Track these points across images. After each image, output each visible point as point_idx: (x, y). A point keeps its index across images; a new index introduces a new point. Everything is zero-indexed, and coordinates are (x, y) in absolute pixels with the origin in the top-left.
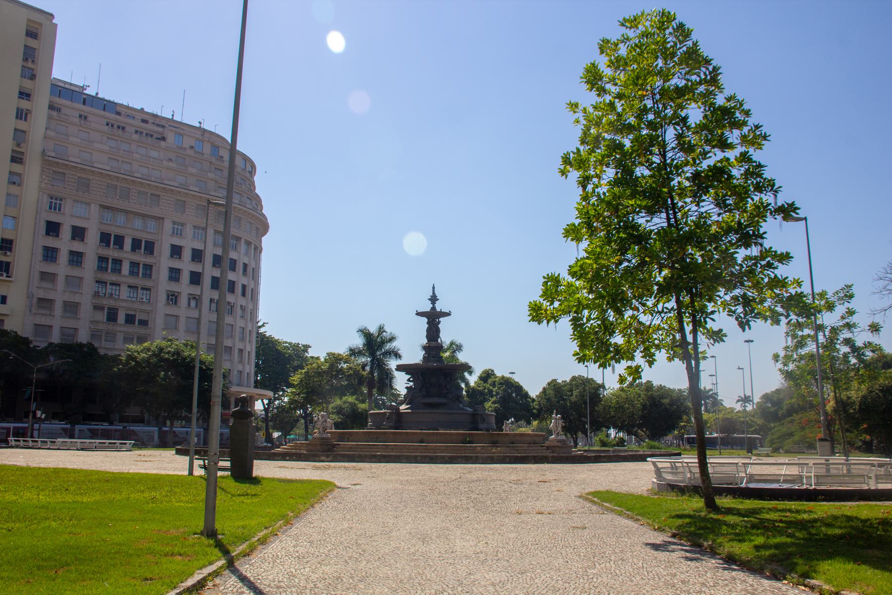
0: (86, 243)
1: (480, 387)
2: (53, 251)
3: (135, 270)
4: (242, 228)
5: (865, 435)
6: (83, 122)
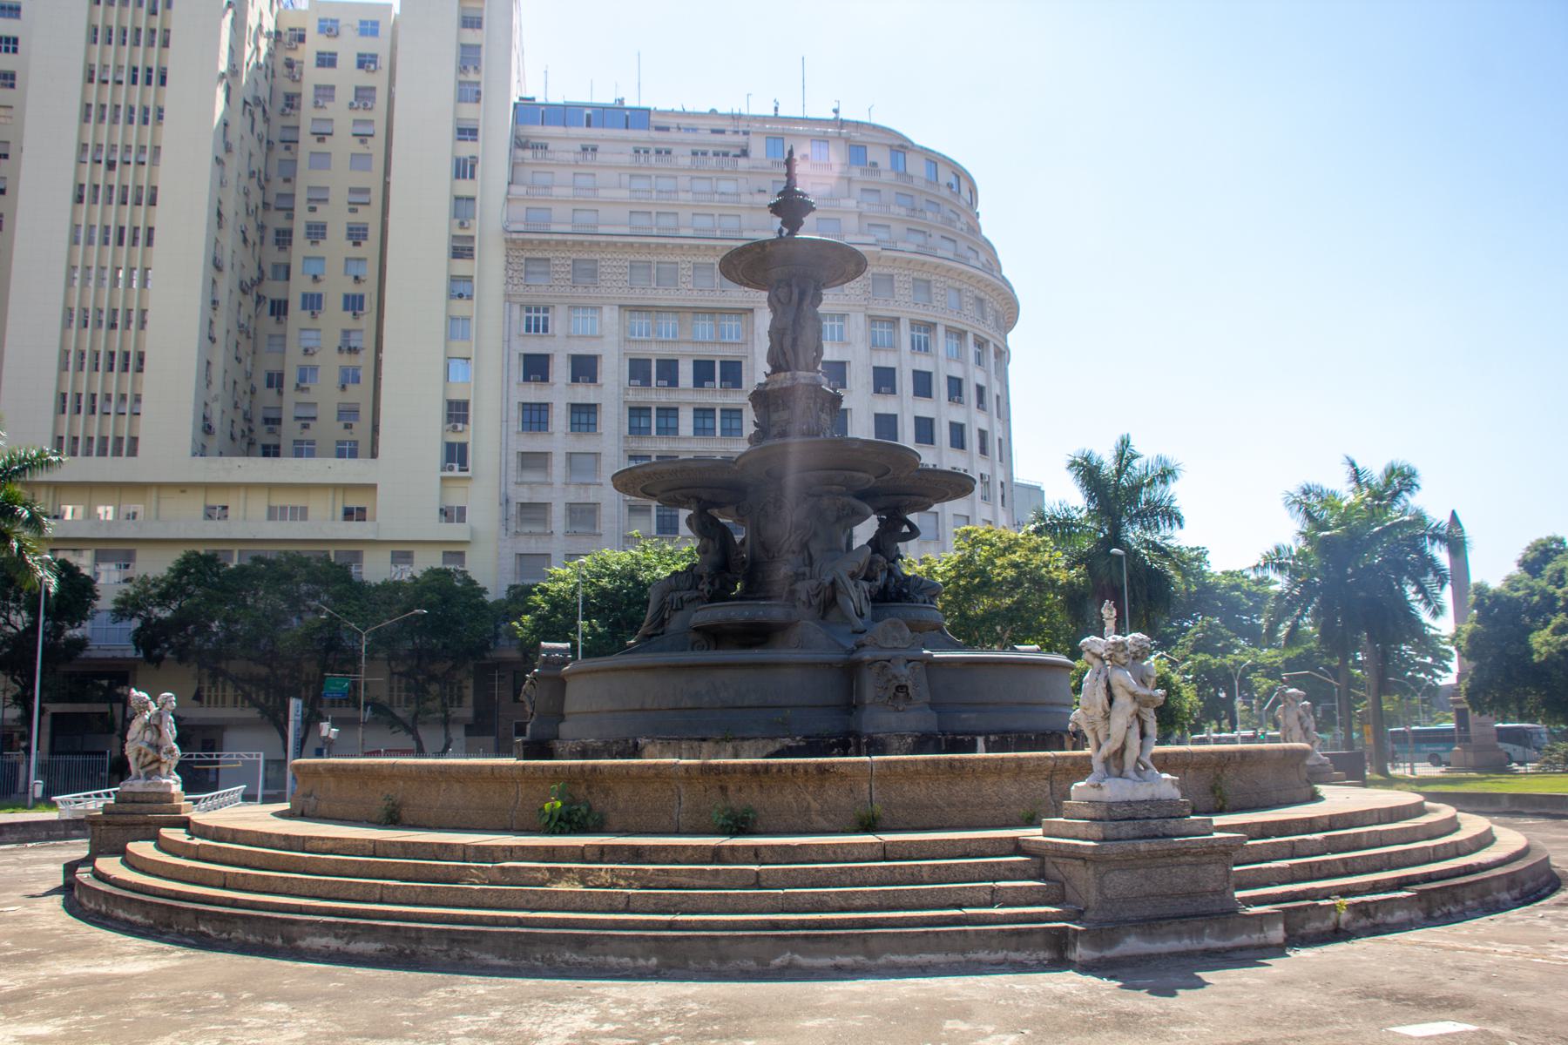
0: (601, 385)
1: (1517, 590)
2: (540, 411)
3: (708, 423)
4: (935, 304)
5: (55, 583)
6: (589, 157)
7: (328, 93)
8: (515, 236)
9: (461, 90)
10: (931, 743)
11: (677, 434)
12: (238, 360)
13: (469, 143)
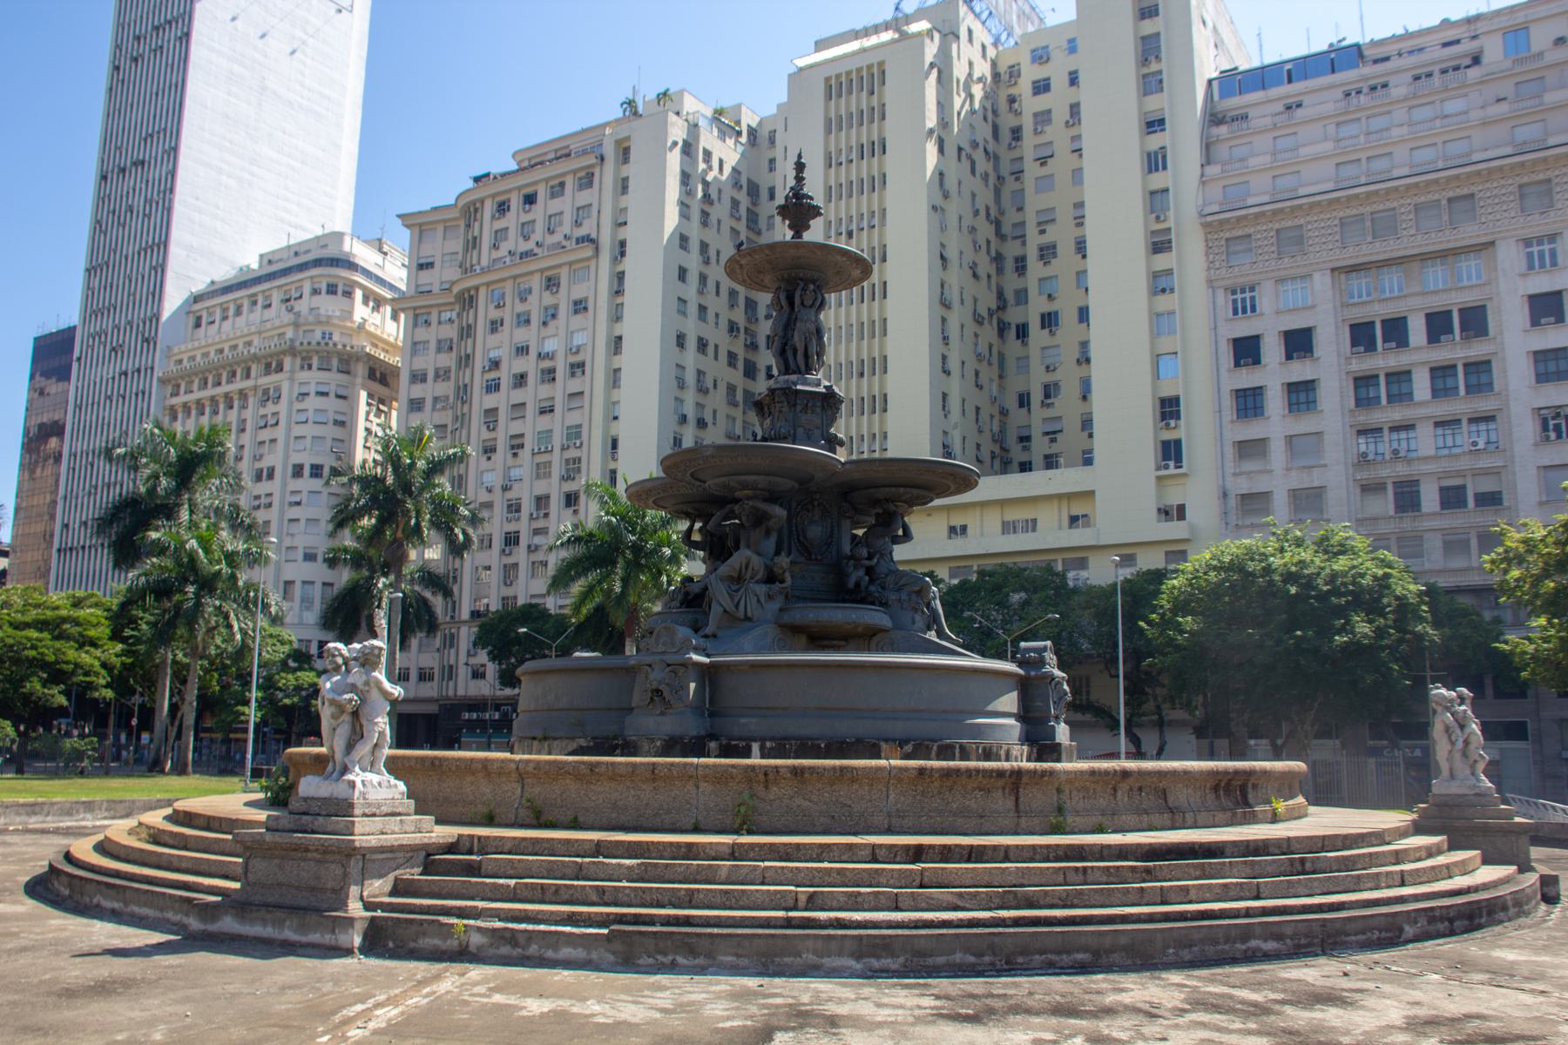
7: (1046, 117)
8: (1209, 219)
9: (1145, 83)
10: (678, 747)
11: (1412, 400)
12: (979, 386)
13: (1158, 135)
